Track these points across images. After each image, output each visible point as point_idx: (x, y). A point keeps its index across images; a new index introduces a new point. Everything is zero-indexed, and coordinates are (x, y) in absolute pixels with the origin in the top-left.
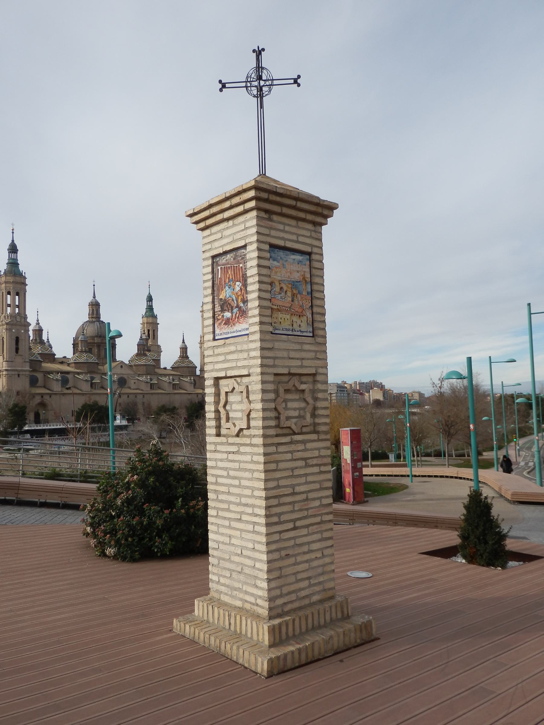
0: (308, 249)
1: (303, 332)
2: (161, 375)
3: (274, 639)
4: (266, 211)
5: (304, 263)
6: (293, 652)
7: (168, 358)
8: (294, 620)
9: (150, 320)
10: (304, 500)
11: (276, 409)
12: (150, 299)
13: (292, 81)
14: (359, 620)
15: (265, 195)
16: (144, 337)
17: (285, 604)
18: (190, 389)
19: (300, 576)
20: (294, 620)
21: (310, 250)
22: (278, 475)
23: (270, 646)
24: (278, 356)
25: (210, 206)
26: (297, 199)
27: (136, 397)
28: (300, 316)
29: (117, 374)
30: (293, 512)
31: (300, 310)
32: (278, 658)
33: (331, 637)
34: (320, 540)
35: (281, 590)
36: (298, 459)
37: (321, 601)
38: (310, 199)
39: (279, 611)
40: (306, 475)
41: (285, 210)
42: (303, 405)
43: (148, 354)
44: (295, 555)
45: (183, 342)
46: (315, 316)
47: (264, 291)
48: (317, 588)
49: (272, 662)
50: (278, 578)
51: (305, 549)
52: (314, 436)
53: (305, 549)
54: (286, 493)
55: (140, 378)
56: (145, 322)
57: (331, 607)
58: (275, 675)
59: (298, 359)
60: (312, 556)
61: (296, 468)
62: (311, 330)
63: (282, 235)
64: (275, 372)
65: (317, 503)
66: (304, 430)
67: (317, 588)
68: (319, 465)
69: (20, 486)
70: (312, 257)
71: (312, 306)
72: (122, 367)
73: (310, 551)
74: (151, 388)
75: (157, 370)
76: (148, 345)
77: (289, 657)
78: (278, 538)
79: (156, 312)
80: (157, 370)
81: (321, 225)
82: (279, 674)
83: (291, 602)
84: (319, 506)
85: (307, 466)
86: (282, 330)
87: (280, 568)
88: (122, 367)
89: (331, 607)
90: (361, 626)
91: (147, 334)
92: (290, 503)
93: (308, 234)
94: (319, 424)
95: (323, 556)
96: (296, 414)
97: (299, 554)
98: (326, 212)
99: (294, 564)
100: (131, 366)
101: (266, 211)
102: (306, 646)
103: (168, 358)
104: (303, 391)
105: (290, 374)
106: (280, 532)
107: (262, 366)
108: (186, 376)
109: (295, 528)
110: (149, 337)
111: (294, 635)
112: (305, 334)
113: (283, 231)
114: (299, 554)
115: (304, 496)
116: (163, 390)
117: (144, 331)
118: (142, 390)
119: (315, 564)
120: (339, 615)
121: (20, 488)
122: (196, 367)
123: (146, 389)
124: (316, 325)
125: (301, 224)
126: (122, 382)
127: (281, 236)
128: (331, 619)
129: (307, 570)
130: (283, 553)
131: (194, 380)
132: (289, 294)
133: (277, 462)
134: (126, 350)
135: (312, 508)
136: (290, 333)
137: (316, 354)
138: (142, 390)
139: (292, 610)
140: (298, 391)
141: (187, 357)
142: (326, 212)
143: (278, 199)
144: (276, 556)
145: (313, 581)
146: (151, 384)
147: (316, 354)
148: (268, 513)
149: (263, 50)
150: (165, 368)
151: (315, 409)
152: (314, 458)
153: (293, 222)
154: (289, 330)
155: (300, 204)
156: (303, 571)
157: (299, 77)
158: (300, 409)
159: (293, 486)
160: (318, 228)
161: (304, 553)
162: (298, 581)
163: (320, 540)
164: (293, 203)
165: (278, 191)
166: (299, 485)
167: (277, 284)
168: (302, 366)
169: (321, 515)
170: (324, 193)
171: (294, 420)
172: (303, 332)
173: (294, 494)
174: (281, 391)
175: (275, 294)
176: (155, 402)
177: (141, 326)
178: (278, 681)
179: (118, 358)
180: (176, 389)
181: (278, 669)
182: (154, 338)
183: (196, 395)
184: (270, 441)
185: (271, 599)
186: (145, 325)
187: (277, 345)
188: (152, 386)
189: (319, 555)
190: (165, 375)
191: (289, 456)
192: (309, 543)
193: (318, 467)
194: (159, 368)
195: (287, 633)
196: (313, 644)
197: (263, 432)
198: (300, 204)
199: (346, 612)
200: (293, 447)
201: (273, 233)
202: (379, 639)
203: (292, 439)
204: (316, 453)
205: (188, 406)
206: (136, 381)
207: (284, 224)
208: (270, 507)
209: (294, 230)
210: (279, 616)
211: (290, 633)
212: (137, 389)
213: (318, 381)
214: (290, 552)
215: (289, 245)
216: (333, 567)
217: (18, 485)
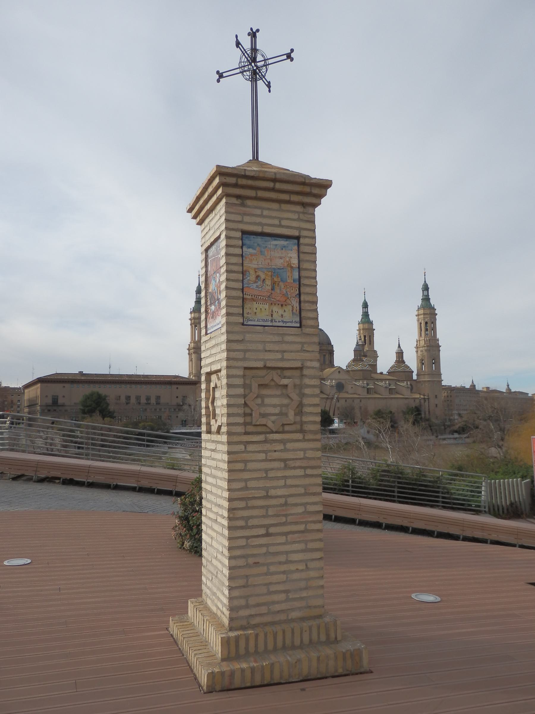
0: (296, 233)
1: (286, 322)
2: (377, 380)
3: (229, 653)
4: (238, 197)
6: (243, 670)
7: (385, 363)
8: (257, 636)
9: (366, 326)
10: (281, 505)
11: (246, 404)
12: (365, 305)
13: (285, 57)
14: (347, 646)
15: (232, 180)
16: (360, 343)
17: (251, 616)
18: (407, 393)
19: (273, 588)
20: (257, 636)
22: (246, 475)
23: (223, 660)
24: (251, 348)
25: (198, 199)
26: (275, 180)
27: (353, 401)
28: (282, 305)
29: (335, 379)
30: (265, 516)
32: (222, 673)
33: (299, 661)
34: (302, 551)
35: (247, 601)
36: (274, 460)
37: (302, 619)
38: (291, 179)
39: (244, 623)
40: (285, 478)
41: (261, 194)
42: (286, 401)
43: (365, 359)
44: (268, 565)
45: (399, 346)
46: (302, 304)
47: (233, 280)
48: (297, 604)
49: (214, 677)
50: (244, 587)
51: (283, 558)
52: (299, 436)
53: (283, 558)
54: (256, 496)
55: (402, 384)
56: (361, 328)
57: (310, 628)
58: (216, 691)
59: (277, 351)
60: (293, 567)
61: (272, 469)
62: (298, 319)
63: (258, 220)
64: (245, 366)
65: (300, 510)
66: (287, 428)
67: (297, 604)
68: (305, 468)
69: (178, 479)
70: (303, 242)
71: (300, 294)
72: (339, 372)
73: (288, 562)
74: (368, 393)
75: (373, 375)
76: (365, 349)
77: (238, 676)
78: (244, 544)
79: (371, 318)
80: (373, 375)
81: (315, 205)
82: (222, 691)
83: (261, 615)
84: (303, 512)
85: (286, 467)
87: (247, 577)
88: (339, 372)
89: (310, 628)
90: (344, 654)
91: (363, 339)
92: (262, 507)
93: (296, 216)
94: (306, 422)
95: (307, 568)
96: (277, 410)
97: (272, 564)
98: (316, 191)
99: (266, 574)
100: (348, 371)
101: (238, 197)
102: (263, 666)
103: (385, 363)
104: (286, 386)
105: (265, 367)
106: (248, 538)
107: (228, 359)
108: (403, 381)
109: (268, 535)
110: (365, 342)
111: (256, 652)
113: (262, 216)
114: (272, 564)
115: (282, 501)
116: (379, 394)
117: (360, 337)
118: (359, 395)
119: (296, 576)
120: (323, 638)
121: (178, 481)
122: (413, 372)
123: (364, 394)
124: (303, 314)
125: (284, 206)
126: (340, 387)
127: (257, 221)
128: (311, 641)
129: (284, 582)
130: (251, 561)
131: (411, 384)
132: (268, 282)
133: (245, 462)
134: (343, 356)
135: (291, 515)
136: (269, 324)
137: (303, 346)
138: (359, 395)
139: (262, 624)
140: (278, 386)
141: (403, 362)
142: (316, 191)
143: (250, 182)
144: (241, 562)
145: (291, 596)
146: (368, 389)
147: (303, 346)
148: (231, 516)
149: (258, 31)
150: (381, 373)
151: (301, 405)
152: (296, 459)
153: (275, 206)
155: (278, 186)
156: (279, 583)
157: (292, 50)
158: (281, 406)
159: (267, 489)
160: (310, 210)
161: (280, 563)
162: (270, 593)
163: (302, 551)
164: (271, 185)
165: (248, 173)
166: (275, 488)
167: (252, 272)
168: (282, 359)
169: (306, 523)
170: (315, 172)
171: (273, 418)
173: (267, 497)
174: (255, 386)
175: (250, 284)
176: (372, 406)
177: (357, 332)
178: (214, 698)
179: (336, 364)
180: (392, 394)
181: (223, 686)
182: (370, 344)
183: (413, 400)
184: (236, 439)
185: (231, 609)
186: (362, 331)
187: (248, 337)
188: (369, 391)
189: (301, 567)
190: (382, 380)
191: (262, 456)
192: (287, 553)
193: (303, 470)
194: (376, 373)
195: (247, 648)
196: (272, 665)
197: (228, 429)
198: (278, 186)
199: (333, 635)
200: (267, 447)
201: (247, 219)
202: (372, 672)
203: (266, 438)
204: (301, 454)
205: (404, 410)
206: (353, 386)
207: (262, 209)
208: (234, 509)
209: (274, 214)
210: (243, 628)
211: (252, 649)
212: (354, 394)
213: (306, 376)
214: (261, 560)
215: (268, 230)
216: (321, 582)
217: (175, 478)
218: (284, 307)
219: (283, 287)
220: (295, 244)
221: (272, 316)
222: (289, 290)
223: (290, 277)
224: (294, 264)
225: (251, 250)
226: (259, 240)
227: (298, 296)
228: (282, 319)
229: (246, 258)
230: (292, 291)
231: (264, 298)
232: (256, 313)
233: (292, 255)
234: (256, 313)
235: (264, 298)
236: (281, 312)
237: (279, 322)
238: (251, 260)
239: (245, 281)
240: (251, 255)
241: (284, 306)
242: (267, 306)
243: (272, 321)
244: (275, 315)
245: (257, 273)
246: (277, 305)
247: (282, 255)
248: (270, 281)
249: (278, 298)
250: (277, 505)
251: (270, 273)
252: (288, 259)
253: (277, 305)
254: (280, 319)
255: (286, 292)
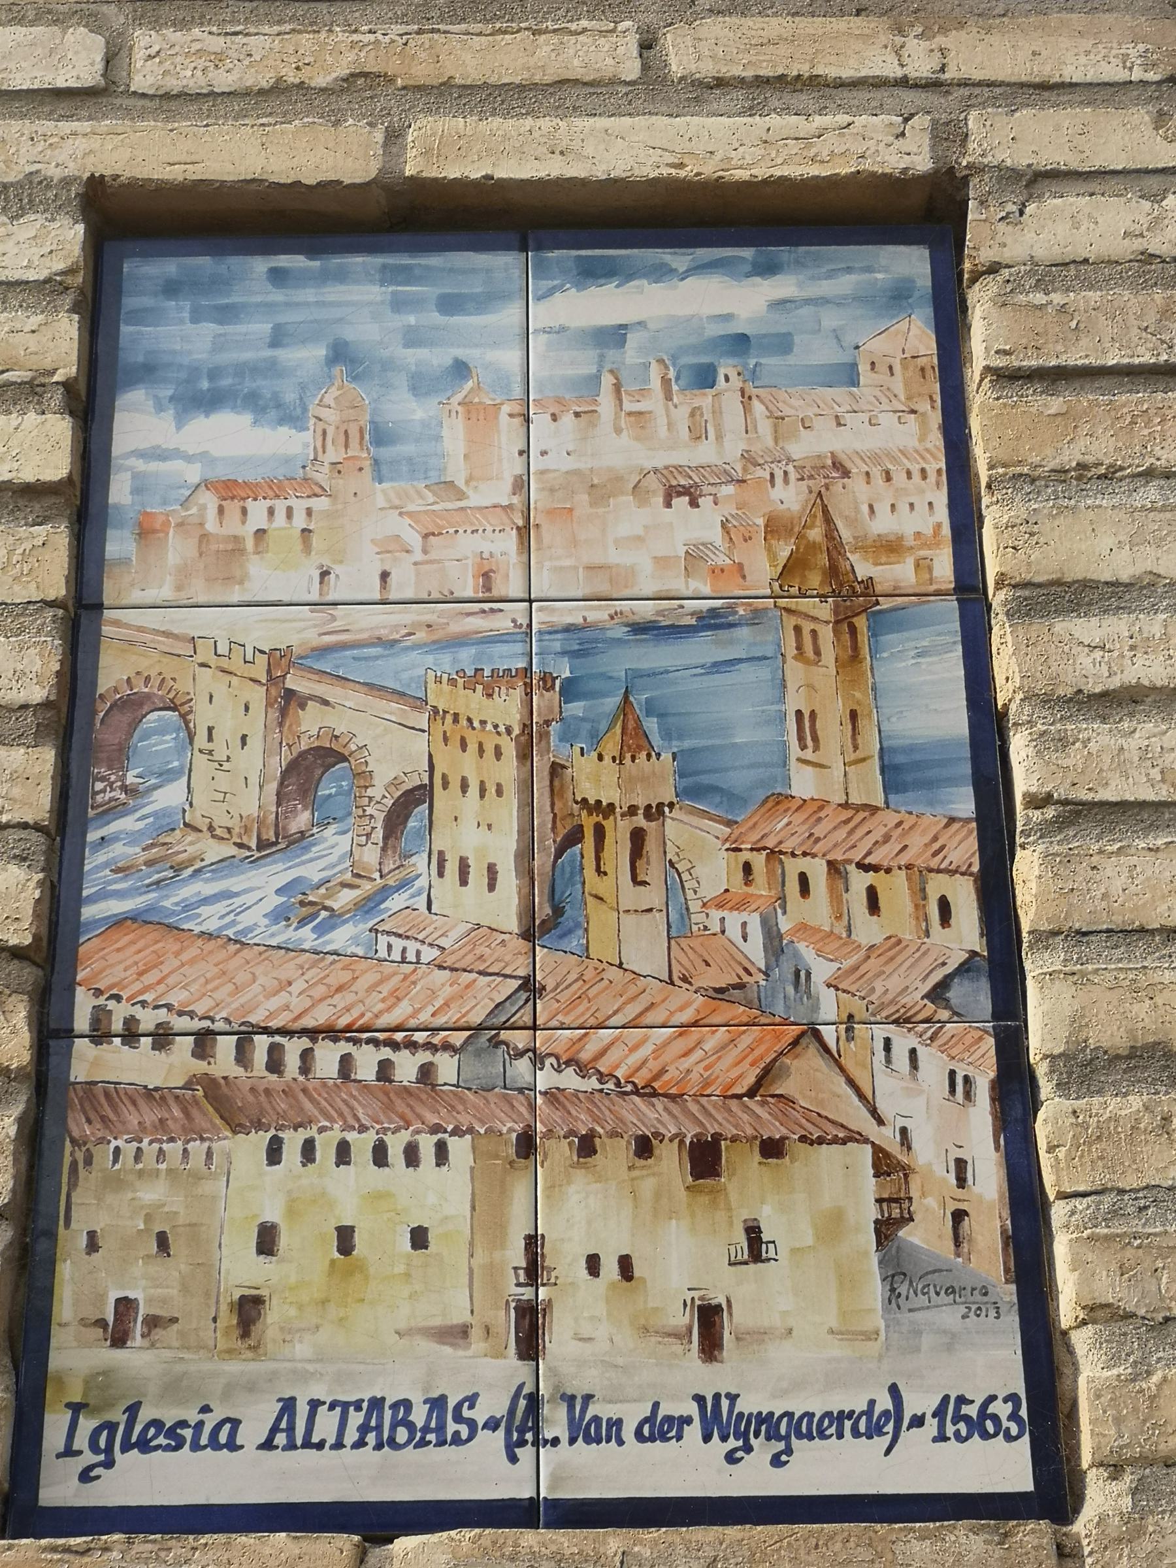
0: (893, 147)
1: (784, 1431)
5: (817, 352)
21: (912, 155)
28: (705, 1159)
31: (724, 1057)
62: (994, 1366)
86: (288, 1430)
112: (819, 1470)
132: (483, 828)
136: (482, 1470)
154: (445, 1423)
167: (229, 711)
170: (126, 1455)
172: (784, 1431)
218: (748, 1186)
219: (714, 872)
220: (897, 297)
221: (530, 1345)
222: (818, 909)
223: (833, 729)
224: (891, 547)
225: (231, 438)
226: (359, 297)
227: (977, 996)
228: (712, 1379)
229: (146, 532)
230: (868, 930)
231: (407, 1067)
232: (249, 1309)
233: (849, 441)
234: (249, 1309)
235: (407, 1067)
236: (685, 1257)
237: (659, 1429)
238: (227, 557)
239: (114, 846)
240: (231, 491)
241: (744, 1173)
242: (442, 1192)
243: (523, 1425)
244: (586, 1338)
245: (311, 724)
246: (615, 1155)
247: (705, 453)
248: (508, 812)
249: (630, 1056)
250: (158, 631)
251: (507, 708)
252: (790, 498)
253: (615, 1155)
254: (684, 1379)
255: (775, 943)
